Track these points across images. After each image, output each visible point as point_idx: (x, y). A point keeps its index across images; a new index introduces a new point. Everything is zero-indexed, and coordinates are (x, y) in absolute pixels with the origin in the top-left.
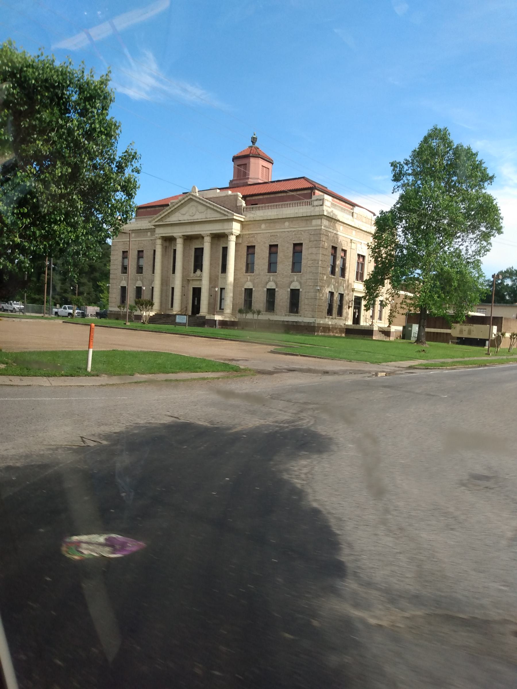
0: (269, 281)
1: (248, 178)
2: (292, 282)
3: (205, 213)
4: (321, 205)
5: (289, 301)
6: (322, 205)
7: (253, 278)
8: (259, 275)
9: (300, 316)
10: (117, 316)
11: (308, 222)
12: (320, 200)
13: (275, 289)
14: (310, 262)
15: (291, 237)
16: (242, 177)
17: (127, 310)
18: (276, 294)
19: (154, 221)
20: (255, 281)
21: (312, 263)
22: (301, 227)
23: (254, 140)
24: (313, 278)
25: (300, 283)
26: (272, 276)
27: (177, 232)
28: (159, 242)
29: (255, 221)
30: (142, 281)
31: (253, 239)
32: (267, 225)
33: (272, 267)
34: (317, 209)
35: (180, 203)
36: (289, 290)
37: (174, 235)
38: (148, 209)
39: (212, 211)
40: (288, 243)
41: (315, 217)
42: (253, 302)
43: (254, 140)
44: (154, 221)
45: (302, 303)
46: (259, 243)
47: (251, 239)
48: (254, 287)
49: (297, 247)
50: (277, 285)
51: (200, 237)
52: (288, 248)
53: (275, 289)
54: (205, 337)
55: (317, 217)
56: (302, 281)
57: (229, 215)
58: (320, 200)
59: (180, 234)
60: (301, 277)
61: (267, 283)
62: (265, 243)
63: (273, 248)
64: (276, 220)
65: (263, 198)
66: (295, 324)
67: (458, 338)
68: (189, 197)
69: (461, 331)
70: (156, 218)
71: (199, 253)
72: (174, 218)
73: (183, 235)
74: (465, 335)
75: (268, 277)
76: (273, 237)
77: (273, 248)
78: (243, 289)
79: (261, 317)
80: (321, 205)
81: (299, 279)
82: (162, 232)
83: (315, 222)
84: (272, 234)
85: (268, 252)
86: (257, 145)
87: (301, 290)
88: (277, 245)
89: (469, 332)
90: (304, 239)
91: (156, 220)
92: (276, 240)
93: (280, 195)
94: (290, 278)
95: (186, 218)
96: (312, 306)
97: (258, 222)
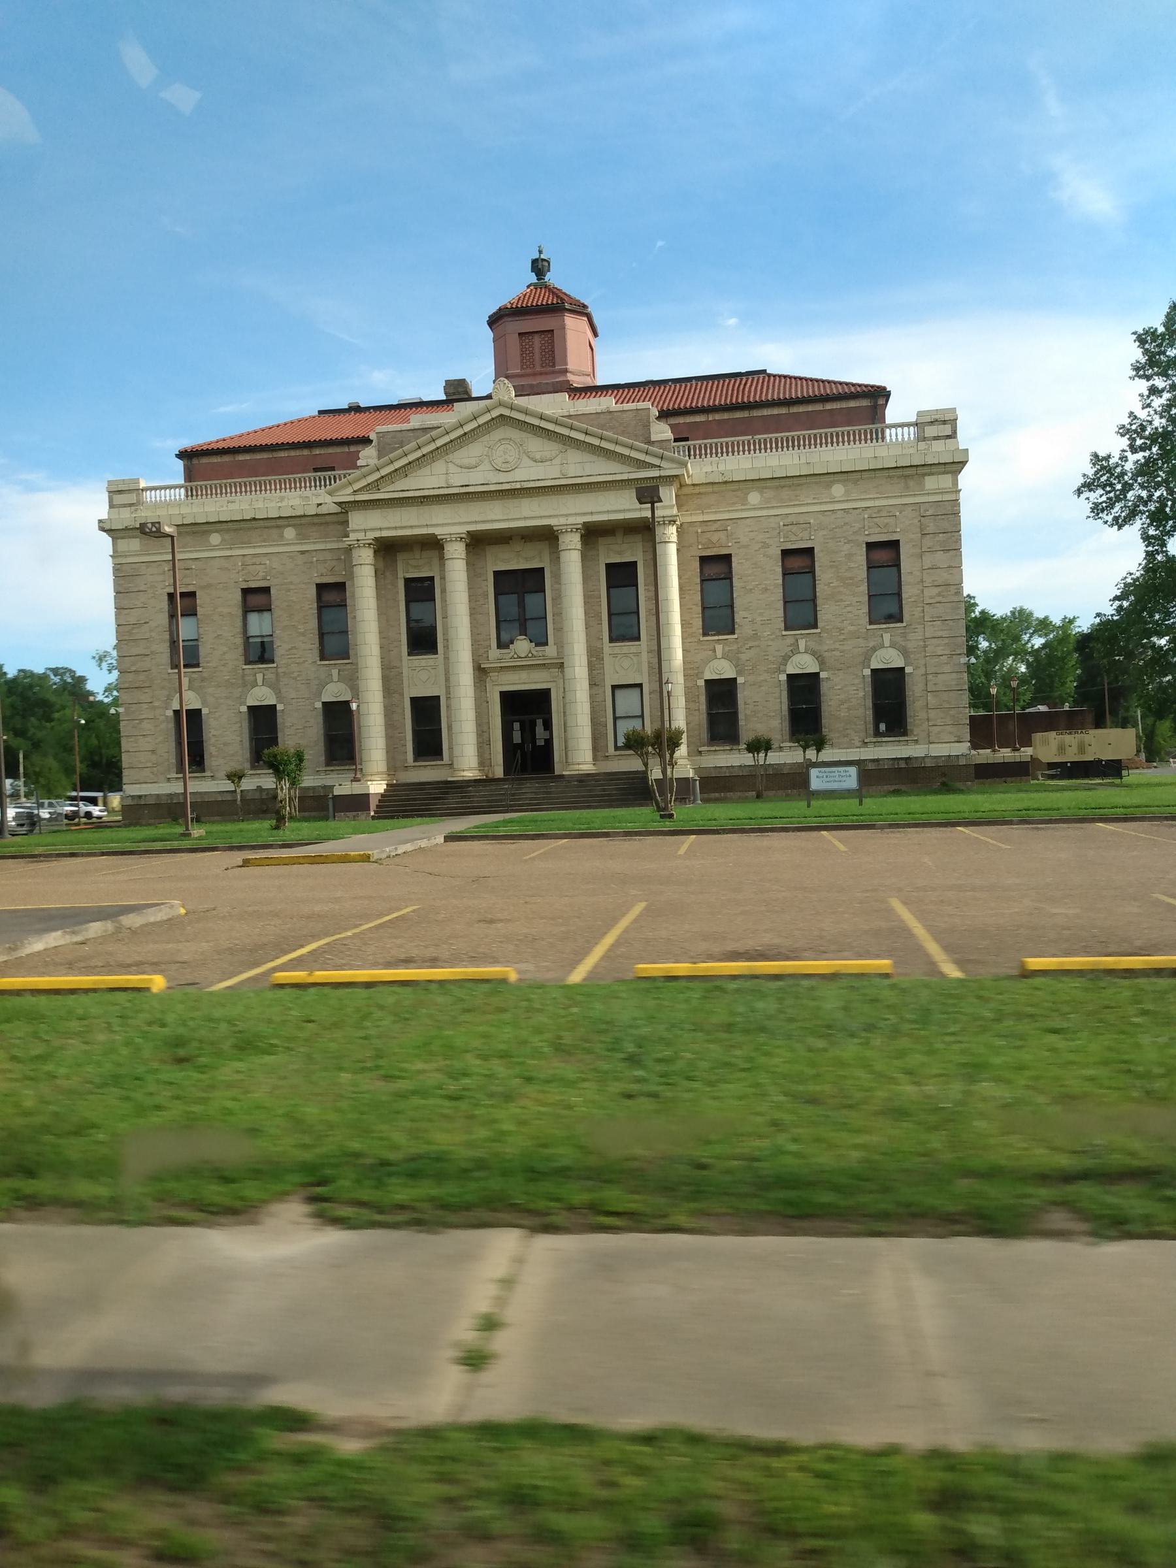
0: (795, 650)
1: (566, 371)
2: (874, 649)
3: (557, 461)
4: (949, 437)
5: (869, 703)
6: (953, 435)
7: (735, 647)
8: (755, 637)
9: (916, 741)
10: (171, 810)
11: (911, 483)
12: (944, 422)
13: (817, 674)
14: (931, 592)
15: (857, 525)
16: (538, 369)
17: (211, 785)
18: (824, 687)
19: (350, 490)
20: (743, 657)
21: (939, 595)
22: (887, 498)
23: (539, 267)
24: (944, 634)
25: (905, 652)
26: (887, 634)
27: (450, 524)
28: (365, 557)
29: (726, 482)
30: (275, 687)
31: (722, 535)
32: (769, 494)
33: (801, 609)
34: (938, 446)
35: (460, 432)
36: (867, 672)
37: (437, 531)
38: (241, 457)
39: (587, 457)
40: (849, 542)
41: (934, 470)
42: (741, 716)
43: (539, 267)
44: (350, 490)
45: (919, 704)
46: (746, 546)
47: (715, 537)
48: (739, 673)
49: (884, 555)
50: (822, 662)
51: (433, 545)
52: (849, 556)
53: (817, 674)
54: (103, 854)
55: (942, 469)
56: (911, 646)
57: (664, 464)
58: (944, 422)
59: (463, 529)
60: (904, 635)
61: (786, 659)
62: (766, 545)
63: (798, 563)
64: (803, 480)
65: (708, 422)
66: (903, 765)
67: (1051, 765)
68: (495, 414)
69: (1062, 749)
70: (358, 480)
71: (421, 592)
72: (429, 480)
73: (376, 539)
74: (1072, 756)
75: (790, 641)
76: (794, 528)
77: (798, 563)
78: (701, 683)
79: (774, 758)
80: (949, 437)
81: (898, 639)
82: (368, 525)
83: (931, 483)
84: (788, 520)
85: (780, 570)
86: (551, 278)
87: (908, 670)
88: (266, 590)
89: (1082, 749)
90: (904, 531)
91: (357, 486)
92: (805, 535)
93: (766, 412)
94: (866, 639)
95: (481, 478)
96: (953, 712)
97: (736, 486)
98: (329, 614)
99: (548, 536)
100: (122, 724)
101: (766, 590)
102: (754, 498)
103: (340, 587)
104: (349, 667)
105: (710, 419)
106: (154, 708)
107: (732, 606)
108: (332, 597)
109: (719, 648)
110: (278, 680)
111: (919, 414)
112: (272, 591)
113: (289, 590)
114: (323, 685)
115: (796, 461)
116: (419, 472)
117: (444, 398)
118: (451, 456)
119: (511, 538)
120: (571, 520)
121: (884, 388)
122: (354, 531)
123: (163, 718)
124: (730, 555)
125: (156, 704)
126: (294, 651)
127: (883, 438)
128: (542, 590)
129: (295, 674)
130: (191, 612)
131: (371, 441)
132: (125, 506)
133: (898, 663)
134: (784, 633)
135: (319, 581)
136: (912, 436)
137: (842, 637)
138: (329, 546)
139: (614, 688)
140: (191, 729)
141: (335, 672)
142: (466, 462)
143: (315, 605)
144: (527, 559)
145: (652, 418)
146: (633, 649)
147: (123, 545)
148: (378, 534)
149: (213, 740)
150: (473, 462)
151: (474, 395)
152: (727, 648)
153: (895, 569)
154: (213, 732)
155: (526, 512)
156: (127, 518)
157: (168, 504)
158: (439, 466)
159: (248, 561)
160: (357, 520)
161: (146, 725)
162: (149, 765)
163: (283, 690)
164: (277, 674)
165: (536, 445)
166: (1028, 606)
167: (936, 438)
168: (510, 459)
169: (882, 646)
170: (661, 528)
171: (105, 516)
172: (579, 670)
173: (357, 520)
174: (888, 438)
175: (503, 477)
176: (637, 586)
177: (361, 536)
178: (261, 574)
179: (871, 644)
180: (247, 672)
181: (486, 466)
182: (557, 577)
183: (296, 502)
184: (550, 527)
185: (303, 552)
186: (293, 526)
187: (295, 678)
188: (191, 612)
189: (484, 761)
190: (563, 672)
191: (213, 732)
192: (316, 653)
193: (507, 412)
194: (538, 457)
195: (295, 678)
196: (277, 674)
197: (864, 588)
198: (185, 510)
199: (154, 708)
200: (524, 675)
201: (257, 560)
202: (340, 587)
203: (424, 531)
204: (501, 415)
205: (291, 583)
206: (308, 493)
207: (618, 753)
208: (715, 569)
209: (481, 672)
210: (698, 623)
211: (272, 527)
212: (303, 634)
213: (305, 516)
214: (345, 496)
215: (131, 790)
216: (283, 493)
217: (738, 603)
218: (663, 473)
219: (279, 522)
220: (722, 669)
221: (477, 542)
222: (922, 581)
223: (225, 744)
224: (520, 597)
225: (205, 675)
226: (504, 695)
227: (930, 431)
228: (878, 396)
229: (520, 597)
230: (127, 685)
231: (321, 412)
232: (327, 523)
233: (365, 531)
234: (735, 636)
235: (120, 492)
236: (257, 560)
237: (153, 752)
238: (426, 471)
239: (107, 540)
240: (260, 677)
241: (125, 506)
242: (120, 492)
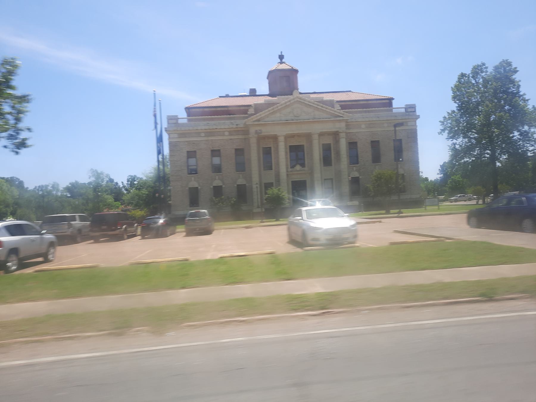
6: (415, 111)
12: (413, 108)
23: (281, 53)
43: (281, 53)
58: (413, 108)
68: (295, 100)
111: (406, 105)
117: (248, 94)
130: (195, 156)
147: (172, 136)
151: (257, 94)
166: (450, 97)
185: (231, 139)
188: (195, 156)
193: (299, 100)
220: (356, 174)
231: (220, 97)
235: (171, 119)
242: (171, 119)
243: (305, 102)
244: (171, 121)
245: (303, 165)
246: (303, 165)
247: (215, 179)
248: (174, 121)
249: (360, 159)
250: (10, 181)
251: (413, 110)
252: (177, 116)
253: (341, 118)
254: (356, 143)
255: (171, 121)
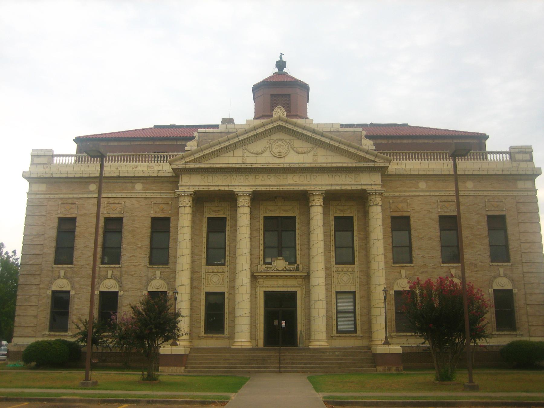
2: (495, 277)
3: (311, 154)
6: (531, 160)
12: (526, 153)
23: (281, 65)
25: (512, 281)
27: (242, 185)
30: (119, 281)
34: (523, 165)
47: (400, 205)
51: (229, 198)
59: (250, 189)
68: (275, 124)
73: (195, 192)
75: (445, 269)
76: (446, 204)
82: (190, 183)
84: (444, 199)
91: (187, 160)
93: (421, 141)
95: (265, 159)
98: (308, 290)
99: (302, 198)
100: (18, 297)
101: (431, 238)
102: (422, 185)
103: (167, 220)
104: (167, 270)
105: (390, 142)
106: (40, 289)
107: (410, 247)
108: (161, 227)
109: (403, 272)
110: (121, 276)
111: (511, 147)
112: (124, 220)
113: (134, 220)
114: (149, 281)
115: (446, 167)
116: (226, 155)
118: (246, 146)
119: (276, 198)
120: (318, 188)
121: (485, 134)
122: (182, 186)
123: (45, 295)
124: (409, 216)
125: (42, 286)
126: (133, 258)
127: (486, 158)
128: (224, 231)
129: (133, 273)
131: (194, 138)
132: (40, 164)
133: (509, 286)
134: (442, 265)
135: (153, 216)
136: (508, 159)
137: (476, 269)
138: (163, 195)
139: (337, 293)
140: (60, 303)
141: (158, 273)
142: (255, 150)
143: (150, 230)
144: (285, 211)
145: (363, 137)
146: (350, 269)
148: (196, 189)
149: (75, 312)
150: (260, 151)
152: (408, 272)
153: (407, 232)
154: (76, 306)
155: (290, 182)
156: (41, 171)
157: (67, 166)
158: (239, 152)
159: (111, 201)
160: (184, 180)
161: (34, 299)
162: (32, 325)
163: (124, 283)
164: (121, 272)
165: (298, 144)
167: (523, 161)
168: (283, 151)
169: (499, 276)
170: (374, 196)
171: (27, 169)
172: (318, 279)
173: (184, 180)
174: (489, 158)
175: (278, 161)
176: (352, 231)
177: (186, 189)
178: (118, 210)
179: (493, 274)
180: (102, 269)
181: (267, 153)
182: (234, 226)
183: (145, 169)
184: (306, 191)
186: (142, 182)
187: (132, 275)
189: (253, 337)
190: (309, 282)
191: (76, 306)
192: (147, 261)
193: (284, 124)
194: (300, 150)
195: (132, 275)
196: (121, 272)
197: (486, 241)
198: (77, 169)
199: (40, 289)
200: (280, 282)
201: (117, 201)
202: (167, 220)
203: (227, 189)
204: (280, 125)
205: (136, 216)
206: (153, 164)
207: (339, 335)
208: (400, 224)
209: (254, 278)
210: (390, 256)
211: (128, 182)
212: (140, 248)
213: (150, 177)
214: (180, 165)
215: (15, 340)
216: (137, 163)
217: (415, 245)
218: (377, 165)
219: (133, 180)
221: (258, 198)
222: (520, 239)
223: (82, 315)
224: (281, 235)
225: (76, 270)
226: (265, 293)
227: (519, 157)
228: (482, 138)
229: (281, 235)
230: (25, 273)
232: (163, 182)
233: (189, 186)
234: (412, 265)
235: (38, 156)
236: (117, 201)
237: (35, 317)
238: (230, 154)
239: (26, 184)
240: (110, 273)
241: (40, 164)
242: (38, 156)
243: (318, 139)
244: (37, 160)
245: (292, 260)
246: (292, 260)
247: (106, 278)
248: (44, 160)
249: (415, 253)
250: (127, 196)
251: (527, 157)
252: (51, 151)
253: (372, 165)
254: (408, 218)
255: (37, 160)
